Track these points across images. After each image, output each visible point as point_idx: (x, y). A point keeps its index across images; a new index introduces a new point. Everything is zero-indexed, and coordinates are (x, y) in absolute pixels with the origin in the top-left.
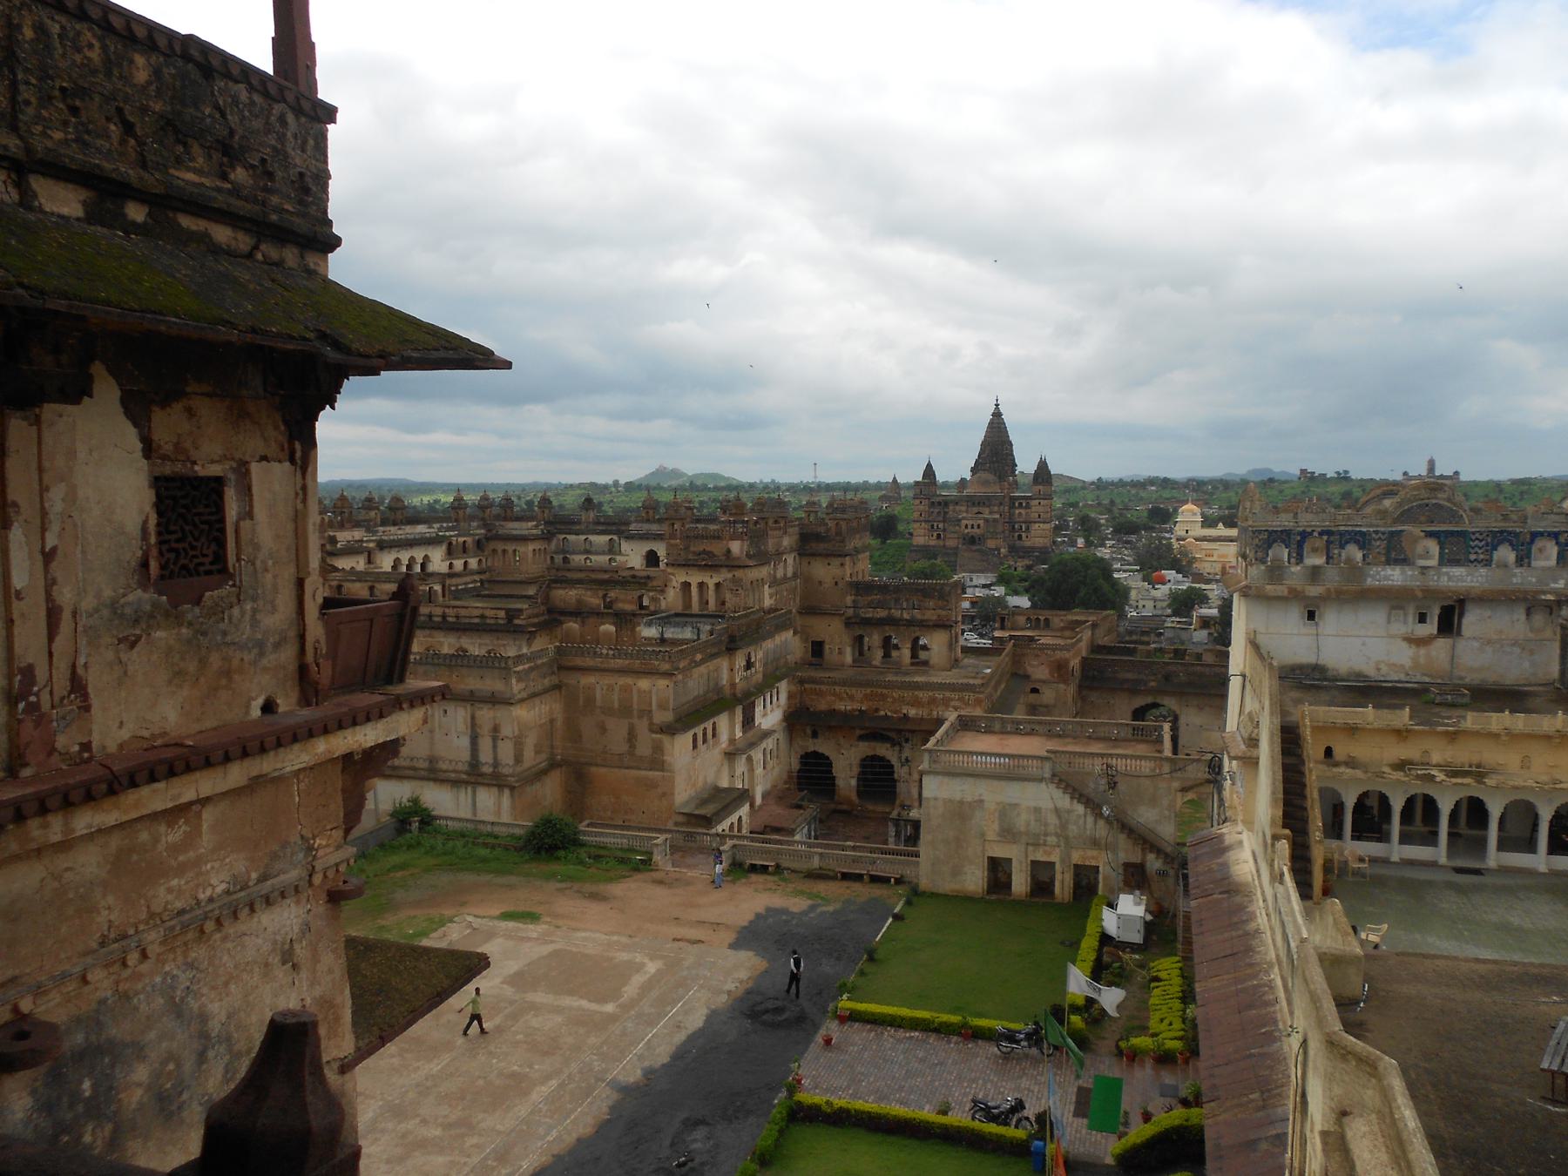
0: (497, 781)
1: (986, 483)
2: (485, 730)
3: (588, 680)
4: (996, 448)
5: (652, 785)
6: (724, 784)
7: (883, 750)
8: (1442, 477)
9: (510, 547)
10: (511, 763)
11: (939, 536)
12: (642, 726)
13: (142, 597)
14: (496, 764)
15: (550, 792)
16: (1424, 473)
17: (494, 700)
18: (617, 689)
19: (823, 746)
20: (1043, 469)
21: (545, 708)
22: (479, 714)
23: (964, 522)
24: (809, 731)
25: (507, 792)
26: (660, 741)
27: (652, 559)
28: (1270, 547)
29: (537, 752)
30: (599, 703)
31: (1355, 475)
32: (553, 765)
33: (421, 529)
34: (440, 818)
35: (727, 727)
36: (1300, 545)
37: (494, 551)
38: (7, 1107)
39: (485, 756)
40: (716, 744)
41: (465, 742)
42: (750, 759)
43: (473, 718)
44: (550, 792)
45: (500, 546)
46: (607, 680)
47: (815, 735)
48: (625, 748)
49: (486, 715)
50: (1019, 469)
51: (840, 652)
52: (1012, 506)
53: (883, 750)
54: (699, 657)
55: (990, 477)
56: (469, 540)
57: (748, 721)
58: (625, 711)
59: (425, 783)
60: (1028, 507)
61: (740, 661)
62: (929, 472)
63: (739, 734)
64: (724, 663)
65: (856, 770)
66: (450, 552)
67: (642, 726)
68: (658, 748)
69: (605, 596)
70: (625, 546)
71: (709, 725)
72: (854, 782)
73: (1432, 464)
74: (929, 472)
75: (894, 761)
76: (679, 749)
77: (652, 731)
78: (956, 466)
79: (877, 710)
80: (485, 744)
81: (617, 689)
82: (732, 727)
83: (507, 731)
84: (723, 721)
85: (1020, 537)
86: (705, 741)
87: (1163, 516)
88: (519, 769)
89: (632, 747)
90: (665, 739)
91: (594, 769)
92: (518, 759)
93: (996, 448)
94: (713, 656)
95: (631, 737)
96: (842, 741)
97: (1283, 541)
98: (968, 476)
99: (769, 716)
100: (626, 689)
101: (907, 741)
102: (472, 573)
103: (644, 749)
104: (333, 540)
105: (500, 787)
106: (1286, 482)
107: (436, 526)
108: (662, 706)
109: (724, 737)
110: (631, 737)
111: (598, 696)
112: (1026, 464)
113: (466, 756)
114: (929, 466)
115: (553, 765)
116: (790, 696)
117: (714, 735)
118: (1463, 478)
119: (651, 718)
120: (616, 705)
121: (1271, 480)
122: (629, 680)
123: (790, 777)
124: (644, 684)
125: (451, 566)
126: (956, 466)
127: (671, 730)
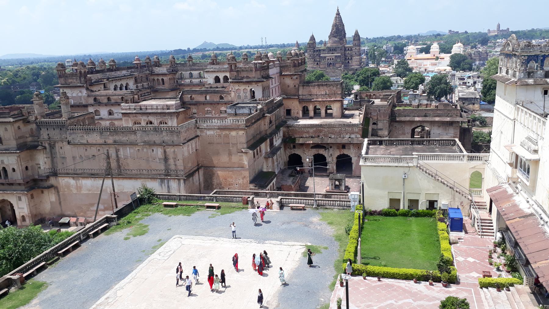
6: (265, 170)
7: (322, 152)
8: (503, 30)
9: (160, 78)
11: (317, 64)
13: (463, 231)
16: (496, 29)
20: (357, 36)
22: (167, 150)
27: (217, 80)
28: (528, 63)
31: (469, 31)
33: (124, 72)
36: (542, 61)
37: (154, 80)
40: (261, 155)
43: (165, 152)
50: (347, 36)
51: (298, 113)
53: (322, 152)
59: (147, 180)
62: (313, 38)
63: (269, 150)
66: (136, 81)
69: (191, 97)
70: (206, 75)
71: (258, 148)
73: (499, 26)
74: (313, 38)
75: (326, 155)
78: (323, 34)
80: (171, 161)
83: (180, 157)
84: (263, 146)
85: (349, 62)
86: (257, 154)
87: (400, 50)
93: (338, 29)
97: (535, 60)
98: (327, 39)
99: (277, 142)
100: (227, 136)
101: (331, 147)
102: (146, 88)
106: (444, 35)
107: (130, 70)
109: (263, 152)
112: (350, 34)
113: (162, 167)
114: (313, 36)
117: (260, 151)
118: (510, 30)
121: (439, 35)
122: (227, 132)
123: (285, 164)
125: (137, 87)
126: (323, 34)
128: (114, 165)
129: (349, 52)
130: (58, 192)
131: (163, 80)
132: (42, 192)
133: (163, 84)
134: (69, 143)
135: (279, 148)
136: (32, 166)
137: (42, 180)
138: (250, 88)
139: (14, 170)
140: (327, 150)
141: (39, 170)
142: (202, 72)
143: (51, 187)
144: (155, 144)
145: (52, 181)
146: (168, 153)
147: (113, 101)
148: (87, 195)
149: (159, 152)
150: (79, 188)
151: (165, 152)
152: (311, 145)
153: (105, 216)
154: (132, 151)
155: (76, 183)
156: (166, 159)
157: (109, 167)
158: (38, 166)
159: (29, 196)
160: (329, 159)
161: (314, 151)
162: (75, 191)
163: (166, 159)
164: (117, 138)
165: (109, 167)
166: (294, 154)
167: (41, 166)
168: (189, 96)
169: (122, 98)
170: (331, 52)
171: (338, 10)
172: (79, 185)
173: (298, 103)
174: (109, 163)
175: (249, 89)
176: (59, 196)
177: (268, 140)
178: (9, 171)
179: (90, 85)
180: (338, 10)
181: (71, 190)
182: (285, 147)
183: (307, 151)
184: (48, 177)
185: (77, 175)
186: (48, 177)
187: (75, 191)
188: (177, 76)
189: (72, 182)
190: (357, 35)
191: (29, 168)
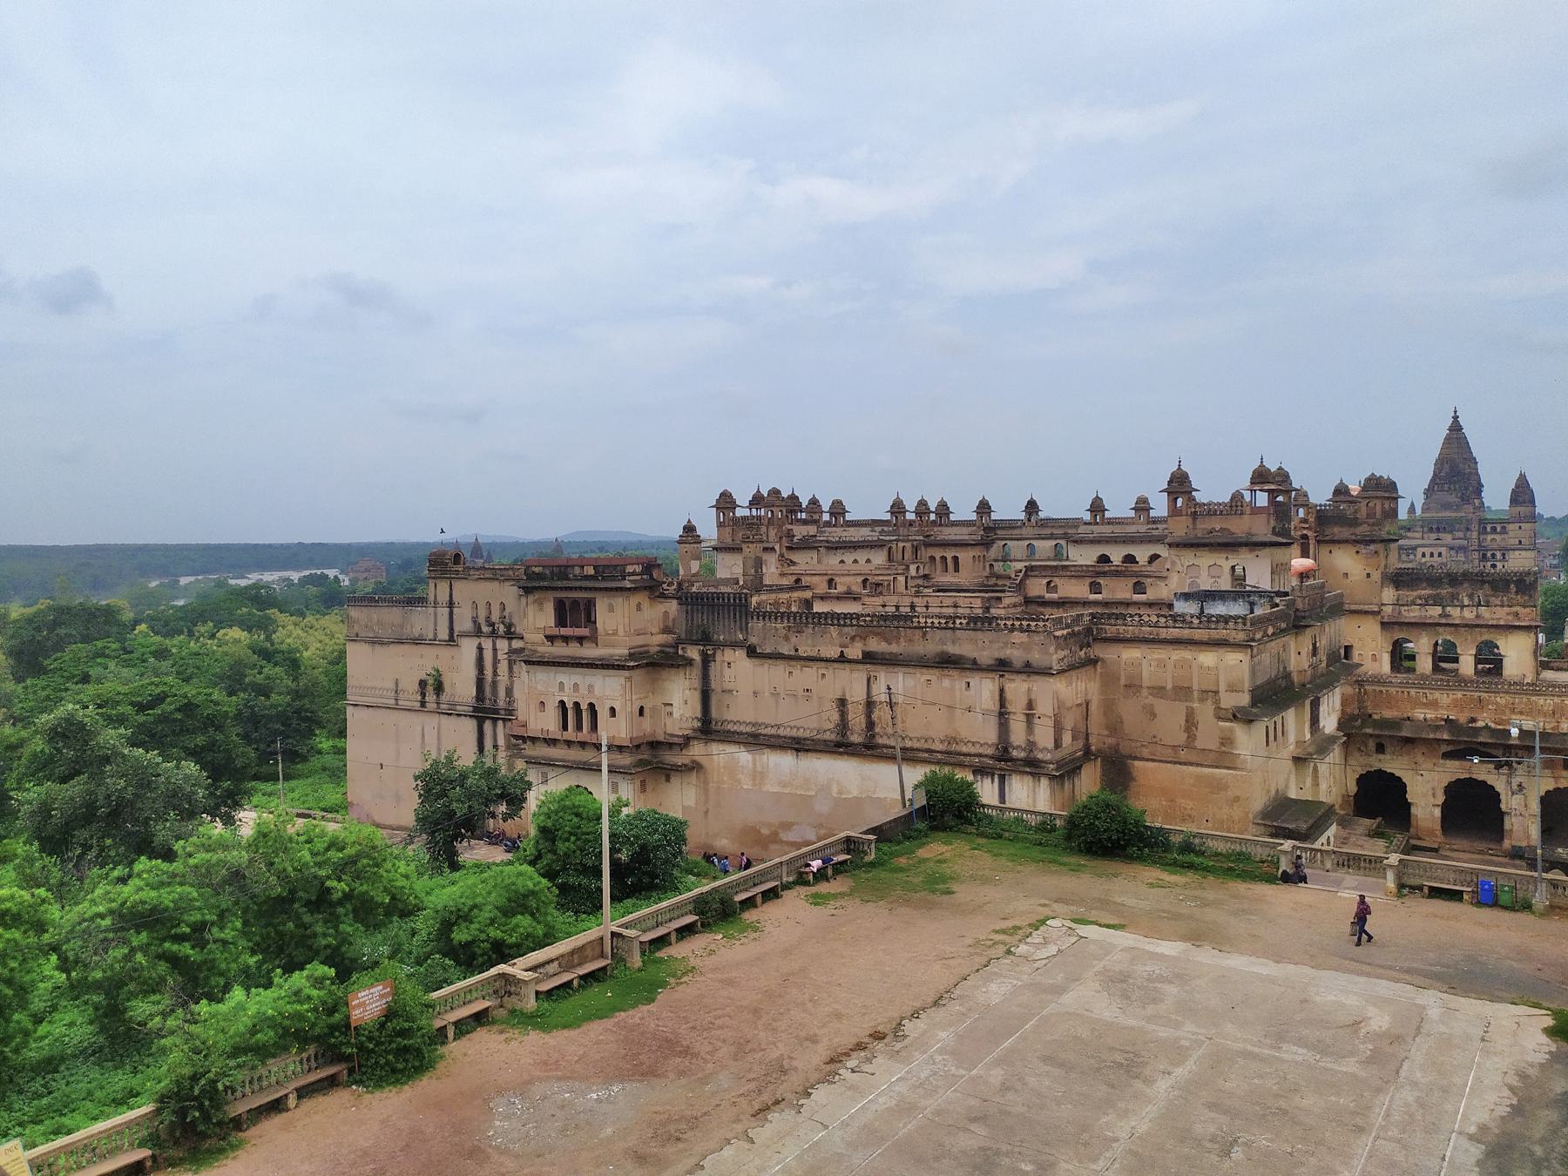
0: (1032, 766)
1: (1446, 506)
2: (1017, 707)
3: (1130, 654)
4: (1456, 469)
5: (1219, 786)
6: (1293, 795)
7: (1479, 769)
9: (949, 554)
10: (1051, 745)
12: (1205, 712)
14: (1031, 745)
15: (1088, 783)
17: (1029, 670)
18: (1170, 667)
19: (1393, 764)
21: (1081, 686)
23: (1420, 551)
24: (1372, 744)
25: (1044, 782)
26: (1231, 730)
29: (1074, 738)
30: (1146, 683)
32: (1088, 754)
34: (984, 806)
35: (1293, 722)
37: (932, 558)
38: (1561, 852)
39: (1018, 735)
41: (993, 723)
42: (1315, 769)
43: (1002, 691)
44: (1088, 783)
45: (938, 553)
46: (1160, 653)
47: (1380, 749)
48: (1182, 738)
49: (1017, 688)
52: (1483, 531)
53: (1479, 769)
54: (1270, 631)
55: (1453, 499)
56: (908, 545)
57: (1315, 721)
58: (1182, 692)
60: (1504, 531)
61: (1307, 648)
63: (1308, 736)
64: (1291, 642)
65: (1441, 799)
67: (1205, 712)
68: (1227, 741)
71: (1278, 719)
72: (1438, 812)
76: (1248, 741)
77: (1219, 718)
79: (1473, 720)
81: (1170, 667)
82: (1300, 731)
83: (1045, 707)
84: (1290, 715)
88: (1059, 755)
89: (1191, 737)
90: (1239, 730)
91: (1136, 763)
92: (1058, 744)
93: (1456, 469)
94: (1281, 632)
95: (1190, 723)
96: (1420, 759)
103: (1207, 738)
104: (790, 535)
105: (1036, 776)
107: (878, 529)
108: (1232, 689)
109: (1292, 738)
110: (1190, 723)
111: (1145, 674)
113: (990, 734)
115: (1088, 754)
116: (1344, 702)
119: (1217, 702)
120: (1169, 687)
124: (1207, 658)
127: (1243, 717)
128: (857, 719)
129: (1498, 537)
130: (706, 782)
131: (956, 559)
132: (668, 780)
133: (957, 569)
134: (752, 652)
135: (1331, 740)
136: (654, 709)
137: (671, 745)
138: (1232, 562)
139: (613, 711)
140: (1505, 770)
141: (669, 722)
142: (1063, 542)
143: (695, 767)
144: (974, 666)
145: (697, 750)
146: (1008, 695)
147: (841, 589)
148: (778, 797)
149: (984, 689)
150: (758, 776)
151: (1002, 691)
152: (1445, 748)
153: (843, 835)
154: (910, 682)
155: (754, 761)
156: (1003, 715)
157: (843, 726)
158: (668, 709)
159: (638, 783)
160: (1509, 802)
161: (1453, 770)
162: (747, 785)
163: (1003, 715)
164: (876, 645)
165: (843, 726)
166: (1380, 771)
167: (675, 710)
168: (1045, 581)
169: (865, 581)
170: (1434, 536)
171: (1456, 418)
172: (759, 769)
173: (1378, 628)
174: (843, 714)
175: (1227, 565)
176: (706, 791)
177: (1308, 702)
178: (603, 715)
179: (789, 548)
180: (1456, 418)
181: (739, 781)
182: (1346, 745)
183: (1429, 765)
184: (687, 741)
185: (756, 740)
186: (687, 741)
187: (747, 785)
188: (994, 551)
189: (744, 756)
190: (1522, 493)
191: (646, 710)
